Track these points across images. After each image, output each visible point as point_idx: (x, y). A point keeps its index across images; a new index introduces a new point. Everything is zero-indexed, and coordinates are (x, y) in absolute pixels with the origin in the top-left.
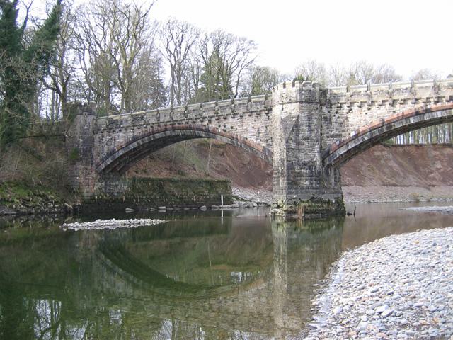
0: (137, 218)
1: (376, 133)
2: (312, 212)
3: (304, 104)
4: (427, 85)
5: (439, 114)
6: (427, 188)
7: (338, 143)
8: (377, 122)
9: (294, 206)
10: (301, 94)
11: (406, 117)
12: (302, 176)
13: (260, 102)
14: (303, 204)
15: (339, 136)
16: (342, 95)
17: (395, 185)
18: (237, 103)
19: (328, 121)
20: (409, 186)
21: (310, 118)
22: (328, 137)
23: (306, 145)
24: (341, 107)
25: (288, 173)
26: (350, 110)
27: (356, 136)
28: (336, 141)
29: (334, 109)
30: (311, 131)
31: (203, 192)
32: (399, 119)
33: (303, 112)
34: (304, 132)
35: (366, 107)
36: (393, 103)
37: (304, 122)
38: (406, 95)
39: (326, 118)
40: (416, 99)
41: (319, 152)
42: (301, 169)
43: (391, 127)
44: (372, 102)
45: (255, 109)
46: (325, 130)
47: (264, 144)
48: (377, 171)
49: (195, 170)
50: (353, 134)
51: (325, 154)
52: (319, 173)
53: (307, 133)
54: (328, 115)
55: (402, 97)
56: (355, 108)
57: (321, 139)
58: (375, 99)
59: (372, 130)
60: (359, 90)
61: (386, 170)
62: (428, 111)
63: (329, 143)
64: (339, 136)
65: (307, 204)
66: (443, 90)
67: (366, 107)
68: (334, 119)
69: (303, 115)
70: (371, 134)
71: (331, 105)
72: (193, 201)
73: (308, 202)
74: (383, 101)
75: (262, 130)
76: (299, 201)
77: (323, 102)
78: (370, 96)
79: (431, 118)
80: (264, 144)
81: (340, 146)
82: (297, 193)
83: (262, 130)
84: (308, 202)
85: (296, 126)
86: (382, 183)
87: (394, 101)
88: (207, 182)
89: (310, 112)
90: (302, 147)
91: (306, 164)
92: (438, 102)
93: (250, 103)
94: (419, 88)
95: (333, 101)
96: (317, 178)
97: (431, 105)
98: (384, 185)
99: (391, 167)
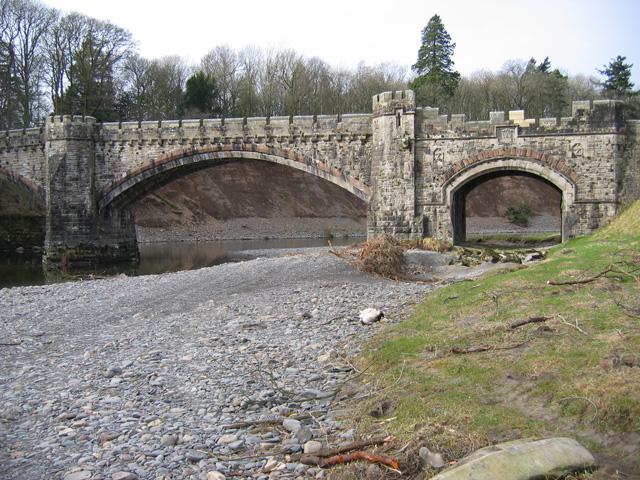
0: (274, 247)
1: (149, 174)
2: (79, 259)
3: (72, 142)
4: (194, 125)
5: (206, 157)
6: (355, 219)
7: (110, 184)
8: (147, 163)
9: (58, 253)
10: (69, 131)
11: (175, 159)
12: (69, 220)
13: (35, 135)
14: (69, 252)
15: (112, 176)
16: (115, 132)
17: (312, 216)
18: (11, 135)
19: (101, 159)
20: (330, 217)
21: (79, 157)
22: (101, 177)
23: (74, 186)
24: (113, 145)
25: (53, 217)
26: (122, 149)
27: (128, 177)
28: (108, 182)
29: (107, 147)
30: (81, 171)
31: (22, 230)
32: (168, 161)
33: (71, 151)
34: (73, 173)
35: (136, 147)
36: (163, 143)
37: (72, 161)
38: (174, 136)
39: (99, 156)
40: (184, 140)
41: (92, 193)
42: (67, 212)
43: (162, 168)
44: (143, 140)
45: (29, 143)
46: (98, 170)
47: (39, 183)
48: (293, 198)
49: (18, 202)
50: (124, 175)
51: (98, 196)
52: (91, 217)
53: (76, 174)
54: (101, 153)
55: (170, 138)
56: (127, 146)
57: (94, 180)
58: (145, 137)
59: (143, 171)
60: (131, 127)
61: (306, 197)
62: (195, 153)
63: (102, 184)
64: (112, 176)
65: (74, 251)
66: (208, 131)
67: (136, 147)
68: (106, 158)
69: (71, 154)
70: (144, 176)
71: (104, 142)
72: (7, 242)
73: (75, 249)
74: (153, 141)
75: (37, 167)
76: (65, 248)
77: (96, 138)
78: (140, 134)
79: (229, 156)
80: (39, 183)
81: (114, 187)
82: (62, 239)
83: (37, 167)
84: (75, 249)
85: (63, 166)
86: (293, 214)
87: (163, 141)
88: (26, 218)
89: (79, 150)
90: (69, 189)
91: (74, 208)
92: (204, 144)
93: (25, 137)
94: (188, 128)
95: (106, 138)
96: (88, 222)
97: (198, 147)
98: (297, 216)
99: (314, 193)
